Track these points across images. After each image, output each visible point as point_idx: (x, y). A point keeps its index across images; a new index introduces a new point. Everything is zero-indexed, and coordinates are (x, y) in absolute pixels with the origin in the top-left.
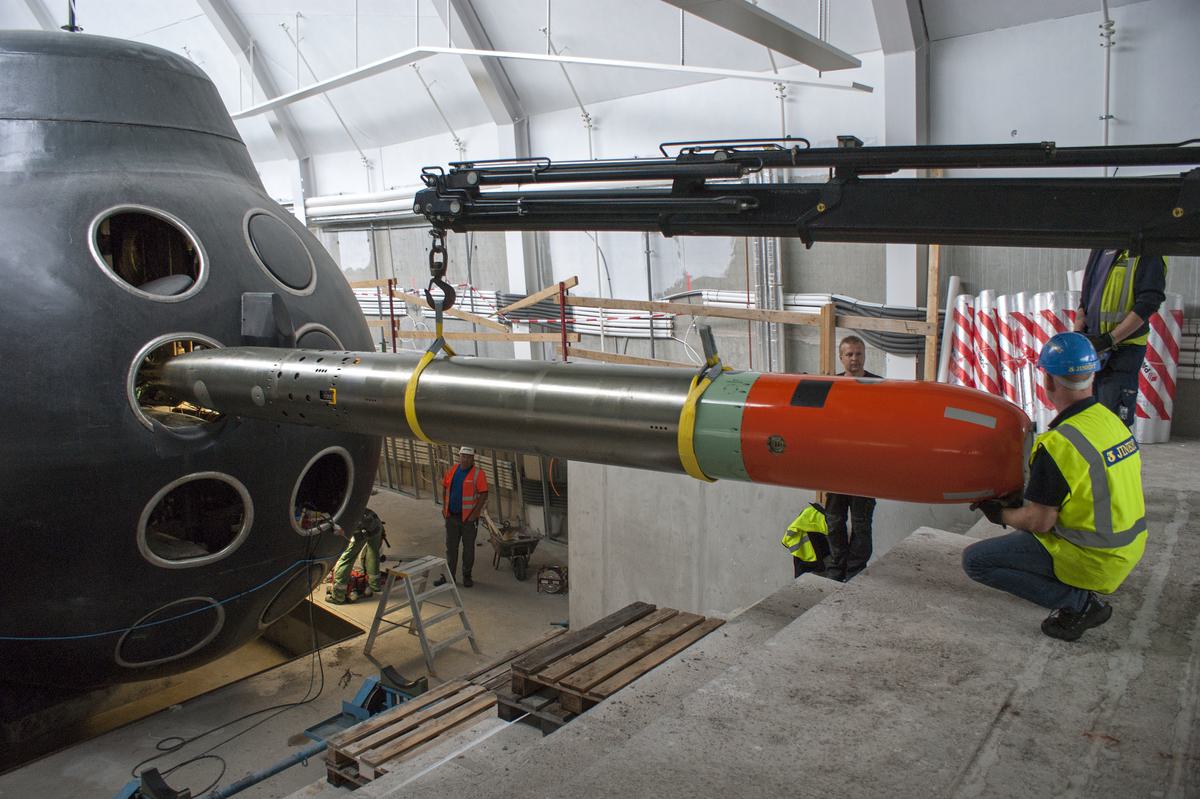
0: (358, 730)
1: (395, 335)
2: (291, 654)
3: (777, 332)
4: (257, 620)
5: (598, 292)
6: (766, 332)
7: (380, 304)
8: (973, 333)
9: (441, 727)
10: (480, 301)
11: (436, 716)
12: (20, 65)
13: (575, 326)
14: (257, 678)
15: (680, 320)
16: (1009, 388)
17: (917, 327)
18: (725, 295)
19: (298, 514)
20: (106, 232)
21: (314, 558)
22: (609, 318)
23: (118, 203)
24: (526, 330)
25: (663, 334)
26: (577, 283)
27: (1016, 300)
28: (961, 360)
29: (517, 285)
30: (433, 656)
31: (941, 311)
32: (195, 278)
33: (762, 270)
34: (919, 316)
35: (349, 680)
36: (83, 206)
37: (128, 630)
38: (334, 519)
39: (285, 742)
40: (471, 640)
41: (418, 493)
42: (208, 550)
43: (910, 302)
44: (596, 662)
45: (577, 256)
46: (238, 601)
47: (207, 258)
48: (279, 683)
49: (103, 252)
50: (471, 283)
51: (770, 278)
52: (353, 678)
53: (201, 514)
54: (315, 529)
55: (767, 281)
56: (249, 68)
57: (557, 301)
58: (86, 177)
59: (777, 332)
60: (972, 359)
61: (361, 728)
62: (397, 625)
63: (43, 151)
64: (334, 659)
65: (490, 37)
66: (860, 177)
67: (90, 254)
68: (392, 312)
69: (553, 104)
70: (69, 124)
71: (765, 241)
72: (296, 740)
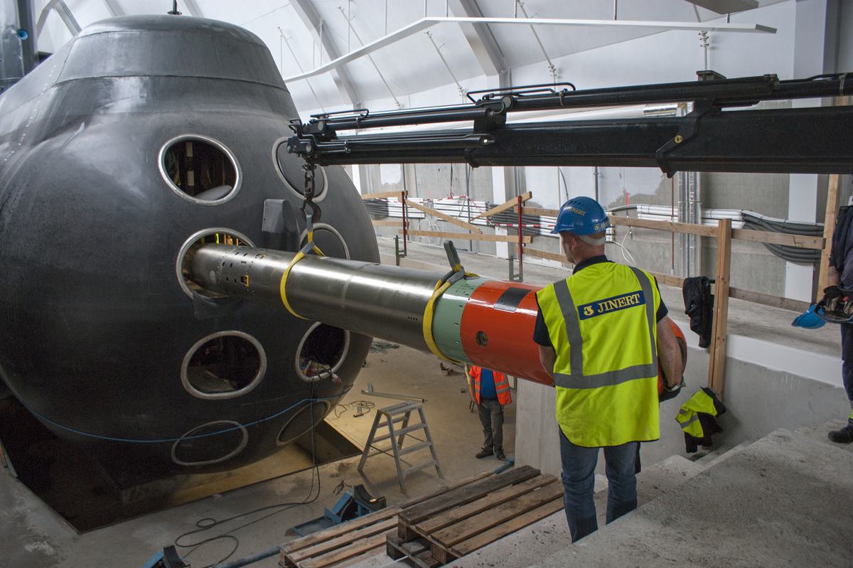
0: (306, 540)
2: (318, 461)
3: (695, 240)
4: (275, 439)
6: (685, 238)
7: (469, 209)
9: (369, 546)
11: (313, 556)
12: (130, 38)
13: (541, 230)
14: (278, 480)
17: (809, 242)
18: (654, 209)
19: (303, 365)
21: (316, 398)
23: (183, 133)
24: (505, 232)
30: (404, 477)
33: (684, 189)
34: (817, 231)
35: (342, 489)
37: (178, 440)
38: (332, 370)
39: (284, 532)
40: (437, 468)
43: (810, 219)
44: (469, 519)
47: (241, 173)
48: (292, 485)
50: (468, 195)
52: (346, 487)
53: (229, 361)
55: (688, 195)
56: (319, 39)
57: (516, 210)
58: (164, 115)
59: (695, 240)
61: (309, 539)
62: (381, 452)
64: (335, 471)
65: (482, 10)
66: (724, 109)
67: (159, 170)
70: (157, 78)
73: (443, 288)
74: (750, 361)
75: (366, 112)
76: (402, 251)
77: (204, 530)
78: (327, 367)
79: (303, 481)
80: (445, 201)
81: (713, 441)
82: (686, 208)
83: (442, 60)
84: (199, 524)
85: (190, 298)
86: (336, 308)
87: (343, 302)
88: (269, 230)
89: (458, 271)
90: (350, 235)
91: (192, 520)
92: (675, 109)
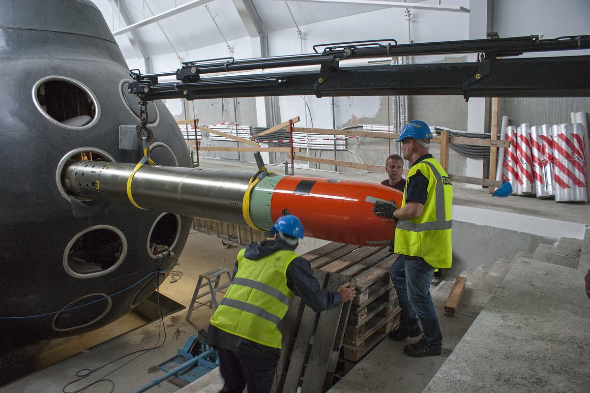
1: (198, 149)
2: (148, 319)
5: (306, 125)
7: (188, 134)
8: (517, 147)
10: (241, 131)
14: (129, 334)
15: (351, 141)
16: (538, 177)
19: (151, 247)
20: (43, 93)
22: (312, 140)
23: (49, 75)
24: (267, 146)
25: (341, 148)
26: (299, 120)
27: (541, 129)
28: (510, 161)
29: (262, 123)
31: (498, 135)
32: (93, 117)
35: (179, 335)
36: (28, 77)
37: (59, 312)
39: (146, 371)
41: (208, 232)
42: (102, 267)
43: (481, 130)
45: (292, 107)
46: (119, 295)
47: (99, 106)
48: (141, 337)
49: (41, 103)
51: (401, 118)
52: (181, 333)
53: (97, 249)
54: (160, 255)
55: (400, 119)
56: (117, 9)
58: (30, 61)
60: (516, 161)
63: (5, 46)
64: (170, 323)
66: (498, 58)
68: (196, 137)
69: (282, 26)
71: (399, 97)
72: (153, 370)
73: (255, 182)
74: (463, 221)
75: (232, 59)
76: (196, 162)
77: (84, 378)
78: (166, 247)
79: (148, 332)
80: (219, 126)
81: (442, 274)
82: (399, 126)
83: (167, 40)
84: (78, 374)
85: (69, 202)
86: (174, 200)
87: (179, 196)
88: (126, 148)
89: (264, 171)
90: (172, 152)
91: (72, 372)
92: (391, 60)
